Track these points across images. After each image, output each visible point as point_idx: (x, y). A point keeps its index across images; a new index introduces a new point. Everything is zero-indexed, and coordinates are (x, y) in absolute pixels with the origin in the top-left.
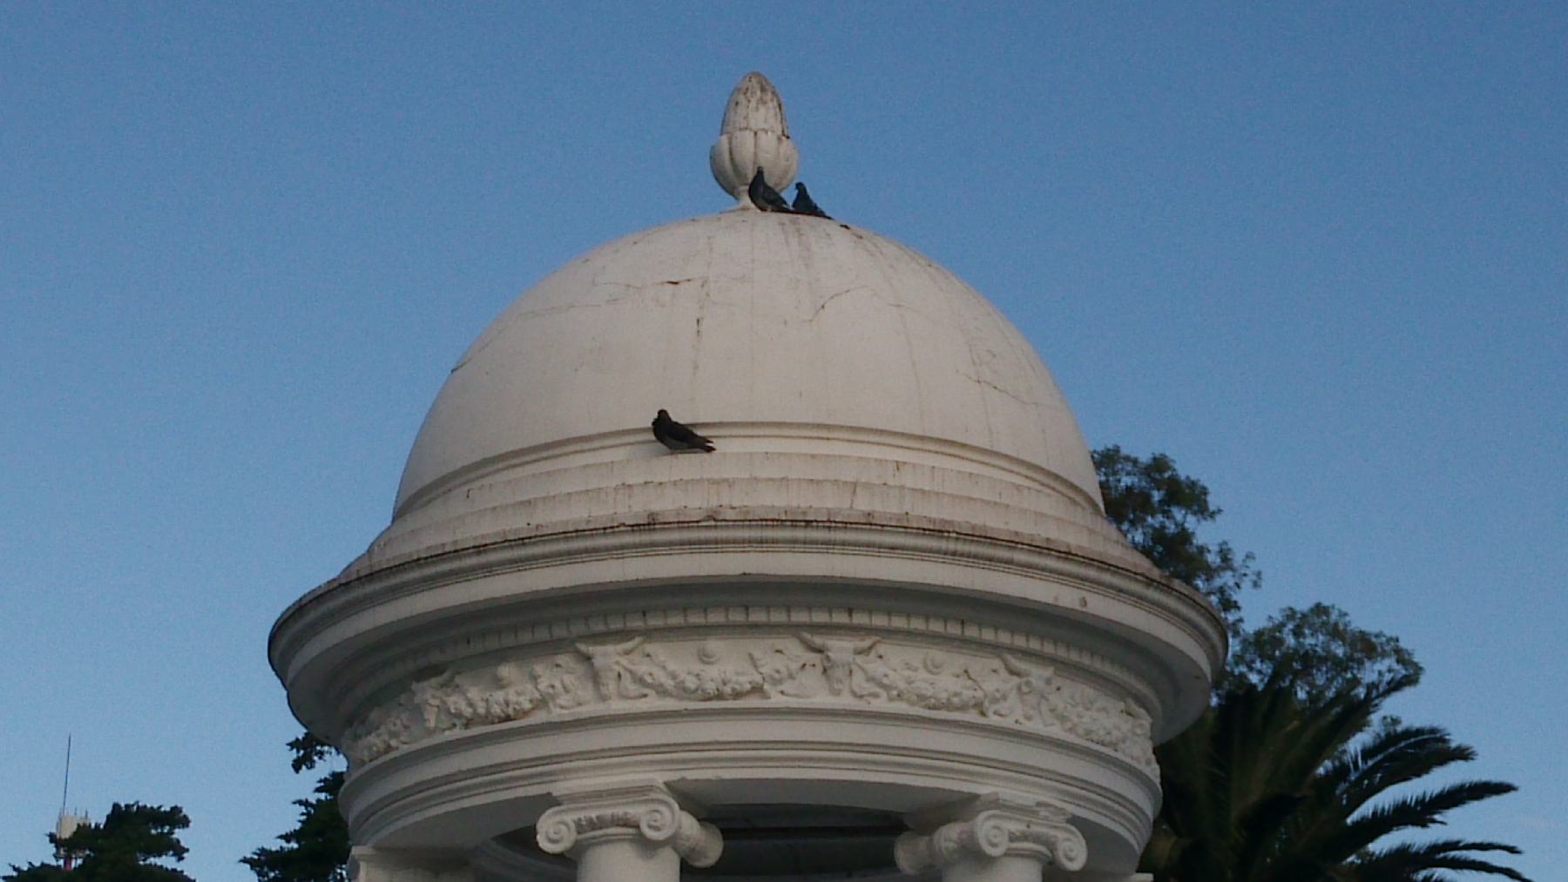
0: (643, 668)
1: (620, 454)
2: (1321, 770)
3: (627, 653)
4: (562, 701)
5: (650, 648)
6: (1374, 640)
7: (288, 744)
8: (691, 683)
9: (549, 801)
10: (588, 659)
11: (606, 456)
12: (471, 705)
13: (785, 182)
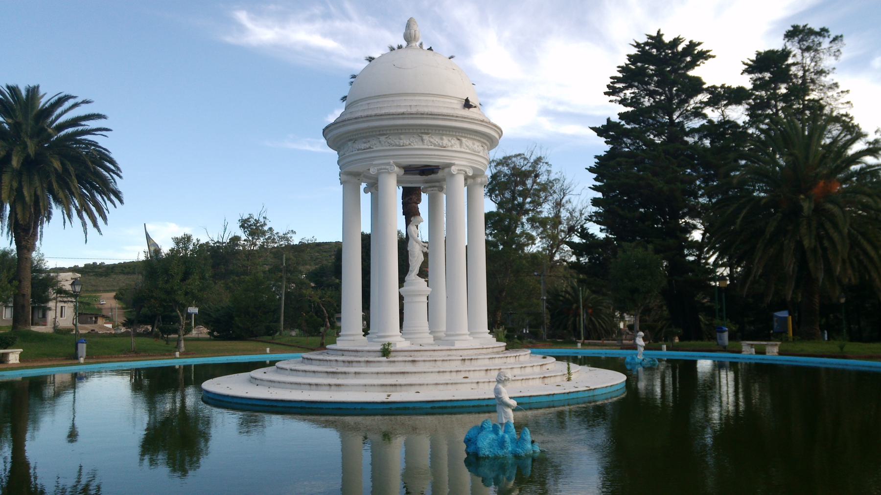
0: (432, 140)
1: (456, 102)
2: (865, 214)
3: (386, 138)
4: (455, 146)
5: (468, 141)
6: (5, 104)
7: (628, 55)
8: (398, 143)
9: (453, 164)
10: (421, 137)
11: (452, 101)
12: (437, 142)
13: (47, 222)
